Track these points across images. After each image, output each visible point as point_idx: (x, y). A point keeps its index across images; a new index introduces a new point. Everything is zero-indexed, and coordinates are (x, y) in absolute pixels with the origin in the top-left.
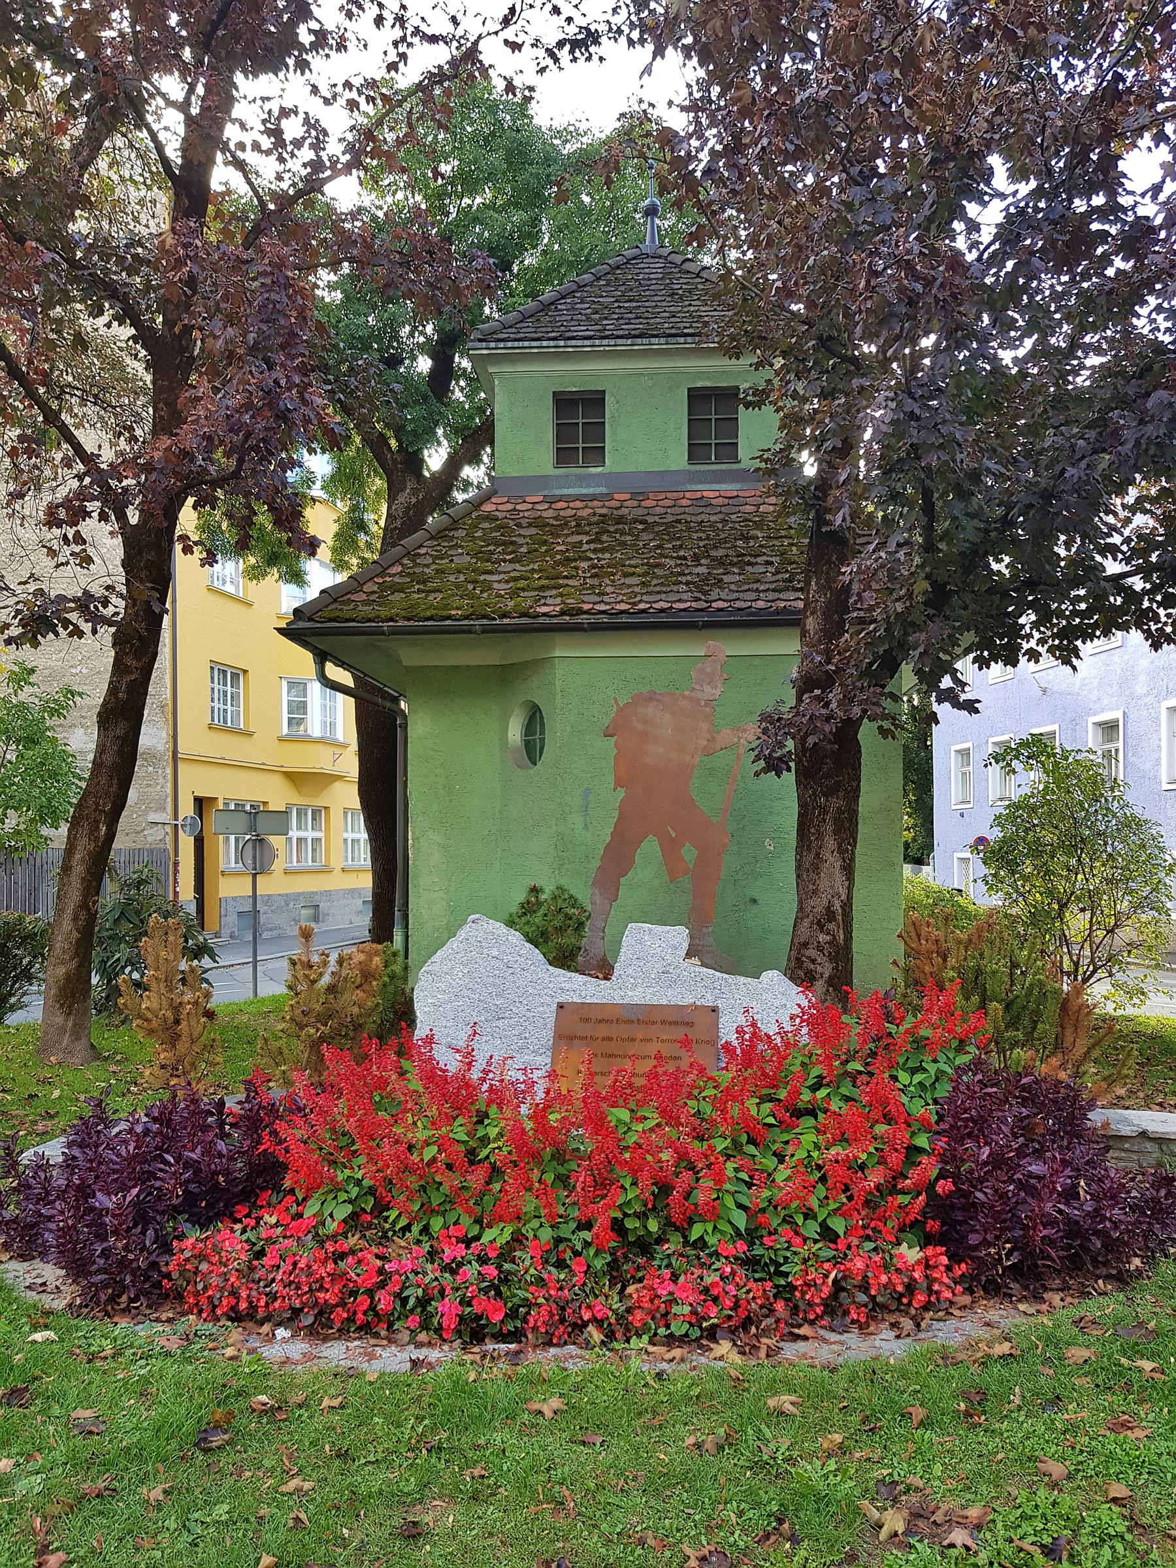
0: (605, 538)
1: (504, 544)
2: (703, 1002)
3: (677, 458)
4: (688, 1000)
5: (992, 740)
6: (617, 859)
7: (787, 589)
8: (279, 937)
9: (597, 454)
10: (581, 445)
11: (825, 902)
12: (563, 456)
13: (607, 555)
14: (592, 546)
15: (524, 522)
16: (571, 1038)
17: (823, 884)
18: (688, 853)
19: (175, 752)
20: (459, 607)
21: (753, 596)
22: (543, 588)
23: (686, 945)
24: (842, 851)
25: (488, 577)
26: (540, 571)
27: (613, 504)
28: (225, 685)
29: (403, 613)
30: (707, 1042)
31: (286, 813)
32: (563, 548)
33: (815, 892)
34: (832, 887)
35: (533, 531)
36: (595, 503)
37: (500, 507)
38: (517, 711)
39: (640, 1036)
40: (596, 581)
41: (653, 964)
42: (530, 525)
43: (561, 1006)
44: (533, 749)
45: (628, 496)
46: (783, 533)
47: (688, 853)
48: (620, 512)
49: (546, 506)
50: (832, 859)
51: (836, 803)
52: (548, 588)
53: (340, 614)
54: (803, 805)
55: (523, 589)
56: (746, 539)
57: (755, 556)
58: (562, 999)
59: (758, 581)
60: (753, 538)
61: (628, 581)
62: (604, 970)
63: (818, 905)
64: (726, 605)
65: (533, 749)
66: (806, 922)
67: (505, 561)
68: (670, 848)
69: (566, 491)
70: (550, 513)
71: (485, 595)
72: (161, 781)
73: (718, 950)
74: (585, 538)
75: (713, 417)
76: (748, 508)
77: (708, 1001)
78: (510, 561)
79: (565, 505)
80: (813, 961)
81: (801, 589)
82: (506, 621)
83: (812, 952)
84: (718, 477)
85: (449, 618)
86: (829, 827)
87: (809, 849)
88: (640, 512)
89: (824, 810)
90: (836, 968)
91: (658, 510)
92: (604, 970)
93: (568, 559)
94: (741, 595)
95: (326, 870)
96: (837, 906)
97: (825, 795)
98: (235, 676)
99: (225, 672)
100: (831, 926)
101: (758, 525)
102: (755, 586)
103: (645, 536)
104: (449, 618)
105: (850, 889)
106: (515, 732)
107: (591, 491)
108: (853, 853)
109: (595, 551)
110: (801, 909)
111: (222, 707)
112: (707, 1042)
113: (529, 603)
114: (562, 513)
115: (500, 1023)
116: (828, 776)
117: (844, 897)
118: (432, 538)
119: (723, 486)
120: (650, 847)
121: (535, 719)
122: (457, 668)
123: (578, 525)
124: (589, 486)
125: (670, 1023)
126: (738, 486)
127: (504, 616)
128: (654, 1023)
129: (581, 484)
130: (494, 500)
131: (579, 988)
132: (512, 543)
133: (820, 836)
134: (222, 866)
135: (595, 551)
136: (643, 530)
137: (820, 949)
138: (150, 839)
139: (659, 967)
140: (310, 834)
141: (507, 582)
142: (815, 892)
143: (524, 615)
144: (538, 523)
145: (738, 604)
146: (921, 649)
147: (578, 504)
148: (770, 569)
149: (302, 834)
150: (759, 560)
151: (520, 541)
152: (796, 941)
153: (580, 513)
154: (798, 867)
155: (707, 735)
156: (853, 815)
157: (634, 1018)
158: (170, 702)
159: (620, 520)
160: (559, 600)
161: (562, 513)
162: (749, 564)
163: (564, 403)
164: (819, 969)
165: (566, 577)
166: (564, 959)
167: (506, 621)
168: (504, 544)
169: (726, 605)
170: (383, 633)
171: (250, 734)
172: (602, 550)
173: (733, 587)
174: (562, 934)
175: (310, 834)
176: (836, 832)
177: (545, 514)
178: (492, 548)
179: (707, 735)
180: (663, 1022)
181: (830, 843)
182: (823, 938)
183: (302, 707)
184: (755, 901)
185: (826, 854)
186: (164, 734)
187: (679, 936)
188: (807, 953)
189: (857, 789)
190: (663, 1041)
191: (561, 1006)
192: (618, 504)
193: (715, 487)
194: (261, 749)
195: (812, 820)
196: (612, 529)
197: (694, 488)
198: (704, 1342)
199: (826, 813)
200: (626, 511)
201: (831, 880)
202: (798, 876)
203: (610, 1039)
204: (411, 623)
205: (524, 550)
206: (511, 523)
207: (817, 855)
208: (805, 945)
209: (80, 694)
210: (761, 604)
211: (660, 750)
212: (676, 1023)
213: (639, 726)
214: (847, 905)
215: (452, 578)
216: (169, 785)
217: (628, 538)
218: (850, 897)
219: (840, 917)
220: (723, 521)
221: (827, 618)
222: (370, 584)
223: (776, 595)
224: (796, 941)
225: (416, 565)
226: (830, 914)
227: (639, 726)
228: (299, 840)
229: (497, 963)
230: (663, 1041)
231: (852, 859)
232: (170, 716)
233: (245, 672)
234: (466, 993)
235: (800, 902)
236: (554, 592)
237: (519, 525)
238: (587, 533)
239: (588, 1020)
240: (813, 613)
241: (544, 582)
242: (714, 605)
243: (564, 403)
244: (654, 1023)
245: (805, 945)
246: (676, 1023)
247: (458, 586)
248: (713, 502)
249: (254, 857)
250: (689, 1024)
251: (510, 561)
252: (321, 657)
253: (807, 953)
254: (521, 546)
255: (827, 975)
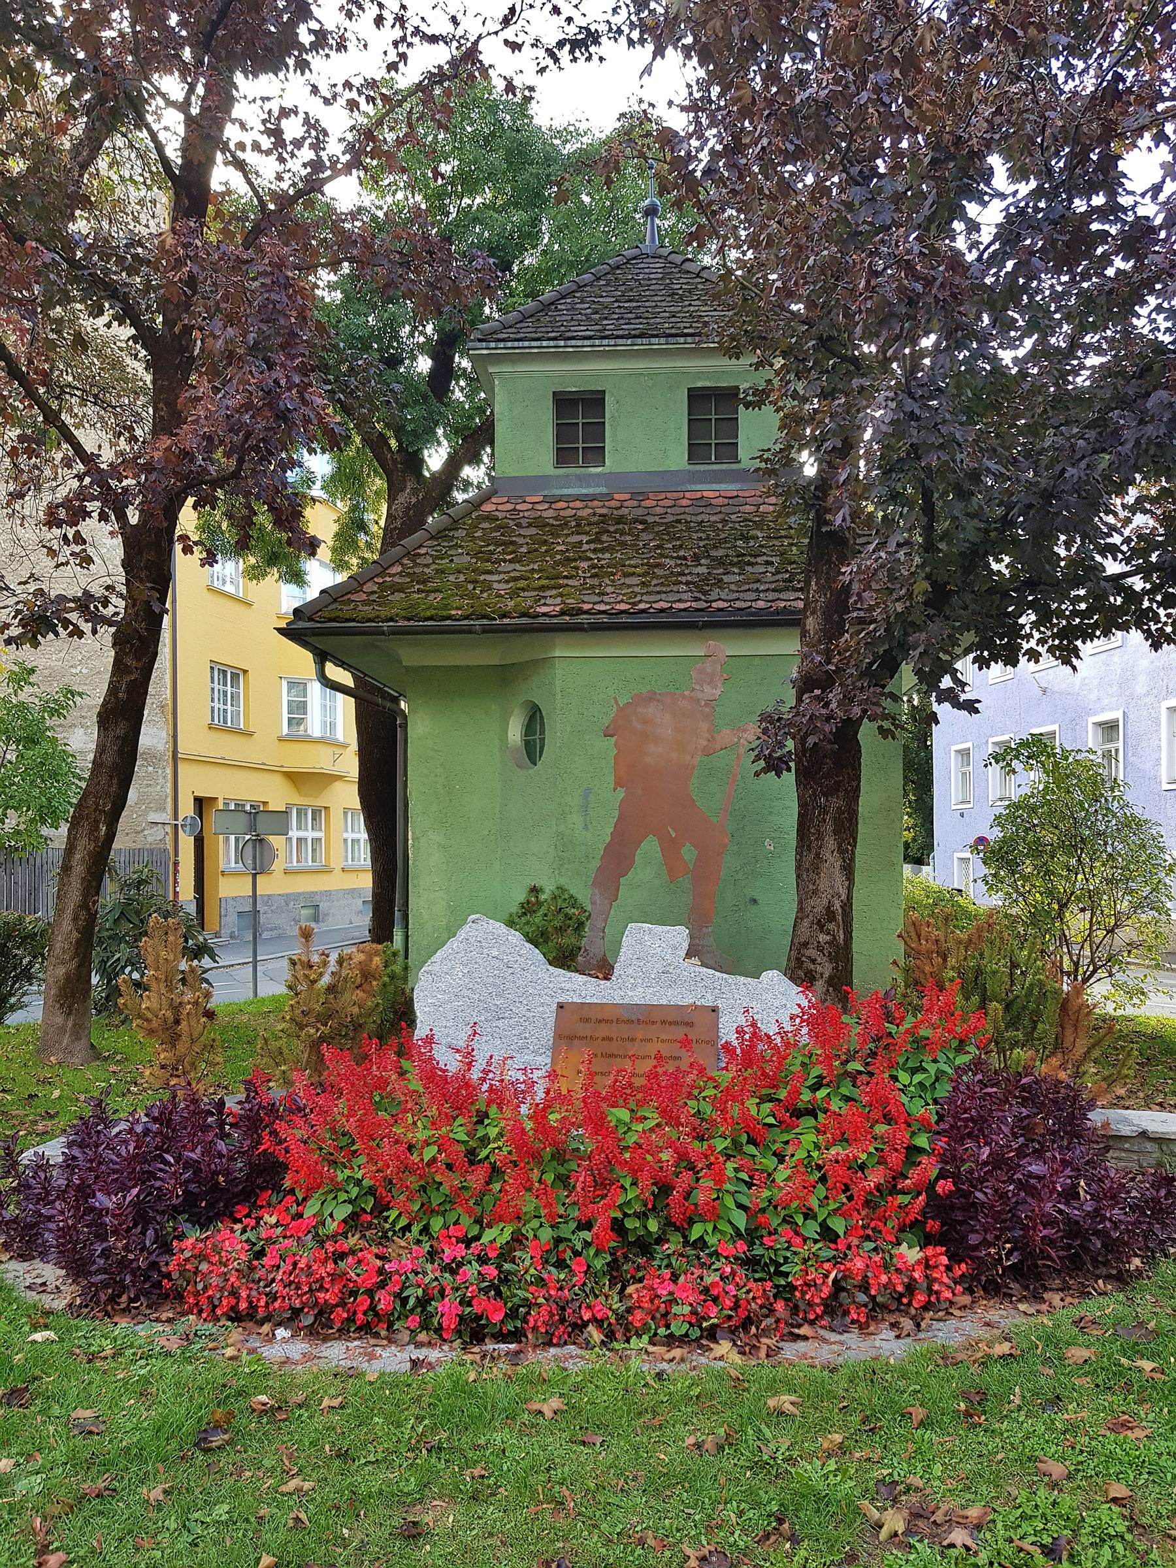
0: (605, 538)
1: (504, 544)
2: (703, 1002)
3: (677, 458)
4: (688, 1000)
5: (992, 740)
6: (617, 859)
7: (787, 589)
8: (279, 937)
9: (597, 454)
10: (581, 445)
11: (825, 902)
12: (563, 456)
13: (607, 555)
14: (592, 546)
15: (524, 522)
16: (571, 1038)
17: (823, 884)
18: (688, 853)
19: (175, 752)
20: (459, 607)
21: (753, 596)
22: (543, 588)
23: (686, 945)
24: (842, 851)
25: (488, 577)
26: (540, 571)
27: (613, 504)
28: (225, 685)
29: (403, 613)
30: (707, 1042)
31: (286, 813)
32: (563, 548)
33: (815, 892)
34: (832, 887)
35: (533, 531)
36: (595, 503)
37: (500, 507)
38: (517, 711)
39: (640, 1036)
40: (596, 581)
41: (653, 964)
42: (530, 525)
43: (561, 1006)
44: (533, 749)
45: (628, 496)
46: (783, 533)
47: (688, 853)
48: (620, 512)
49: (546, 506)
50: (832, 859)
51: (836, 803)
52: (548, 588)
53: (340, 614)
54: (803, 805)
55: (523, 589)
56: (746, 539)
57: (755, 556)
58: (562, 999)
59: (758, 581)
60: (753, 538)
61: (628, 581)
62: (604, 970)
63: (818, 905)
64: (726, 605)
65: (533, 749)
66: (806, 922)
67: (505, 561)
68: (670, 848)
69: (566, 491)
70: (550, 513)
71: (485, 595)
72: (161, 781)
73: (718, 950)
74: (585, 538)
75: (713, 417)
76: (748, 508)
77: (708, 1001)
78: (510, 561)
79: (565, 505)
80: (813, 961)
81: (801, 589)
82: (506, 621)
83: (812, 952)
84: (718, 477)
85: (449, 618)
86: (829, 827)
87: (809, 849)
88: (640, 512)
89: (824, 810)
90: (836, 968)
91: (658, 510)
92: (604, 970)
93: (568, 559)
94: (741, 595)
95: (326, 870)
96: (837, 906)
97: (825, 795)
98: (235, 676)
99: (225, 672)
100: (831, 926)
101: (758, 525)
102: (755, 586)
103: (645, 536)
104: (449, 618)
105: (850, 889)
106: (515, 732)
107: (591, 491)
108: (853, 853)
109: (595, 551)
110: (801, 909)
111: (222, 707)
112: (707, 1042)
113: (529, 603)
114: (562, 513)
115: (500, 1023)
116: (828, 776)
117: (844, 897)
118: (432, 538)
119: (723, 486)
120: (650, 847)
121: (535, 719)
122: (457, 668)
123: (578, 525)
124: (589, 486)
125: (670, 1023)
126: (738, 486)
127: (504, 616)
128: (654, 1023)
129: (581, 484)
130: (494, 500)
131: (579, 988)
132: (512, 543)
133: (820, 836)
134: (222, 866)
135: (595, 551)
136: (643, 530)
137: (820, 949)
138: (150, 839)
139: (659, 967)
140: (310, 834)
141: (507, 582)
142: (815, 892)
143: (524, 615)
144: (538, 523)
145: (738, 604)
146: (921, 649)
147: (578, 504)
148: (770, 569)
149: (302, 834)
150: (759, 560)
151: (520, 541)
152: (796, 941)
153: (580, 513)
154: (798, 867)
155: (707, 735)
156: (853, 815)
157: (634, 1018)
158: (170, 702)
159: (620, 520)
160: (559, 600)
161: (562, 513)
162: (749, 564)
163: (564, 403)
164: (819, 969)
165: (566, 577)
166: (564, 959)
167: (506, 621)
168: (504, 544)
169: (726, 605)
170: (383, 633)
171: (250, 734)
172: (602, 550)
173: (733, 587)
174: (562, 934)
175: (310, 834)
176: (836, 832)
177: (545, 514)
178: (492, 548)
179: (707, 735)
180: (663, 1022)
181: (830, 843)
182: (823, 938)
183: (302, 707)
184: (755, 901)
185: (826, 854)
186: (164, 734)
187: (679, 936)
188: (807, 953)
189: (857, 789)
190: (663, 1041)
191: (561, 1006)
192: (618, 504)
193: (715, 487)
194: (261, 749)
195: (812, 820)
196: (612, 529)
197: (694, 488)
198: (704, 1342)
199: (826, 813)
200: (626, 511)
201: (831, 880)
202: (798, 876)
203: (610, 1039)
204: (411, 623)
205: (524, 550)
206: (511, 523)
207: (817, 855)
208: (805, 945)
209: (80, 694)
210: (761, 604)
211: (660, 750)
212: (676, 1023)
213: (639, 726)
214: (847, 905)
215: (452, 578)
216: (169, 785)
217: (628, 538)
218: (850, 897)
219: (840, 917)
220: (723, 521)
221: (827, 618)
222: (370, 584)
223: (776, 595)
224: (796, 941)
225: (416, 565)
226: (830, 914)
227: (639, 726)
228: (299, 840)
229: (497, 963)
230: (663, 1041)
231: (852, 859)
232: (170, 716)
233: (245, 672)
234: (466, 993)
235: (800, 902)
236: (554, 592)
237: (519, 525)
238: (587, 533)
239: (588, 1020)
240: (813, 613)
241: (544, 582)
242: (714, 605)
243: (564, 403)
244: (654, 1023)
245: (805, 945)
246: (676, 1023)
247: (458, 586)
248: (713, 502)
249: (254, 857)
250: (689, 1024)
251: (510, 561)
252: (321, 657)
253: (807, 953)
254: (521, 546)
255: (827, 975)
